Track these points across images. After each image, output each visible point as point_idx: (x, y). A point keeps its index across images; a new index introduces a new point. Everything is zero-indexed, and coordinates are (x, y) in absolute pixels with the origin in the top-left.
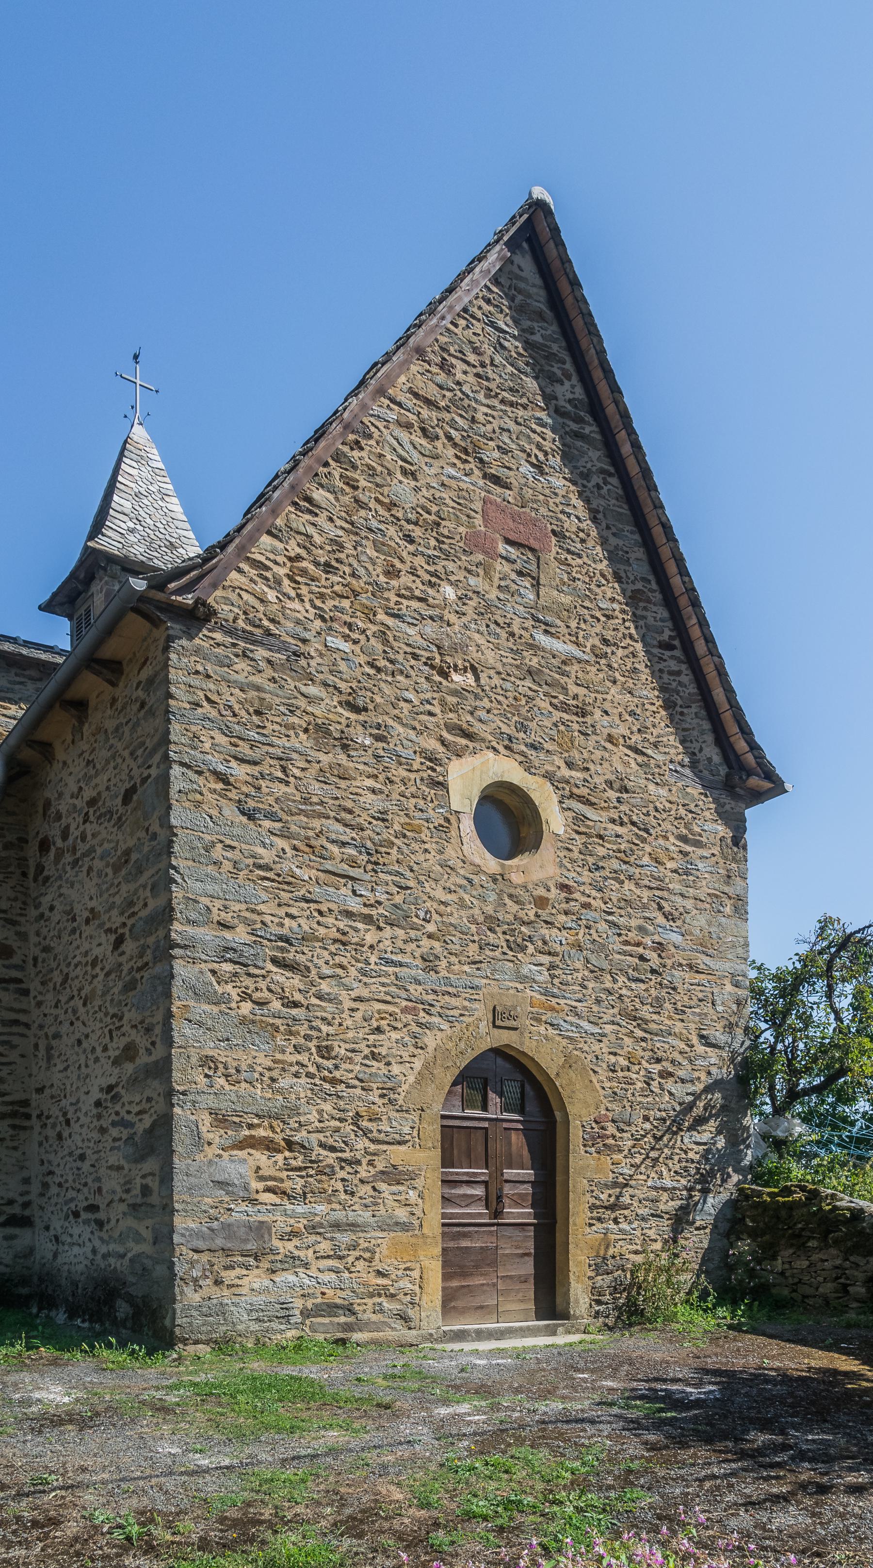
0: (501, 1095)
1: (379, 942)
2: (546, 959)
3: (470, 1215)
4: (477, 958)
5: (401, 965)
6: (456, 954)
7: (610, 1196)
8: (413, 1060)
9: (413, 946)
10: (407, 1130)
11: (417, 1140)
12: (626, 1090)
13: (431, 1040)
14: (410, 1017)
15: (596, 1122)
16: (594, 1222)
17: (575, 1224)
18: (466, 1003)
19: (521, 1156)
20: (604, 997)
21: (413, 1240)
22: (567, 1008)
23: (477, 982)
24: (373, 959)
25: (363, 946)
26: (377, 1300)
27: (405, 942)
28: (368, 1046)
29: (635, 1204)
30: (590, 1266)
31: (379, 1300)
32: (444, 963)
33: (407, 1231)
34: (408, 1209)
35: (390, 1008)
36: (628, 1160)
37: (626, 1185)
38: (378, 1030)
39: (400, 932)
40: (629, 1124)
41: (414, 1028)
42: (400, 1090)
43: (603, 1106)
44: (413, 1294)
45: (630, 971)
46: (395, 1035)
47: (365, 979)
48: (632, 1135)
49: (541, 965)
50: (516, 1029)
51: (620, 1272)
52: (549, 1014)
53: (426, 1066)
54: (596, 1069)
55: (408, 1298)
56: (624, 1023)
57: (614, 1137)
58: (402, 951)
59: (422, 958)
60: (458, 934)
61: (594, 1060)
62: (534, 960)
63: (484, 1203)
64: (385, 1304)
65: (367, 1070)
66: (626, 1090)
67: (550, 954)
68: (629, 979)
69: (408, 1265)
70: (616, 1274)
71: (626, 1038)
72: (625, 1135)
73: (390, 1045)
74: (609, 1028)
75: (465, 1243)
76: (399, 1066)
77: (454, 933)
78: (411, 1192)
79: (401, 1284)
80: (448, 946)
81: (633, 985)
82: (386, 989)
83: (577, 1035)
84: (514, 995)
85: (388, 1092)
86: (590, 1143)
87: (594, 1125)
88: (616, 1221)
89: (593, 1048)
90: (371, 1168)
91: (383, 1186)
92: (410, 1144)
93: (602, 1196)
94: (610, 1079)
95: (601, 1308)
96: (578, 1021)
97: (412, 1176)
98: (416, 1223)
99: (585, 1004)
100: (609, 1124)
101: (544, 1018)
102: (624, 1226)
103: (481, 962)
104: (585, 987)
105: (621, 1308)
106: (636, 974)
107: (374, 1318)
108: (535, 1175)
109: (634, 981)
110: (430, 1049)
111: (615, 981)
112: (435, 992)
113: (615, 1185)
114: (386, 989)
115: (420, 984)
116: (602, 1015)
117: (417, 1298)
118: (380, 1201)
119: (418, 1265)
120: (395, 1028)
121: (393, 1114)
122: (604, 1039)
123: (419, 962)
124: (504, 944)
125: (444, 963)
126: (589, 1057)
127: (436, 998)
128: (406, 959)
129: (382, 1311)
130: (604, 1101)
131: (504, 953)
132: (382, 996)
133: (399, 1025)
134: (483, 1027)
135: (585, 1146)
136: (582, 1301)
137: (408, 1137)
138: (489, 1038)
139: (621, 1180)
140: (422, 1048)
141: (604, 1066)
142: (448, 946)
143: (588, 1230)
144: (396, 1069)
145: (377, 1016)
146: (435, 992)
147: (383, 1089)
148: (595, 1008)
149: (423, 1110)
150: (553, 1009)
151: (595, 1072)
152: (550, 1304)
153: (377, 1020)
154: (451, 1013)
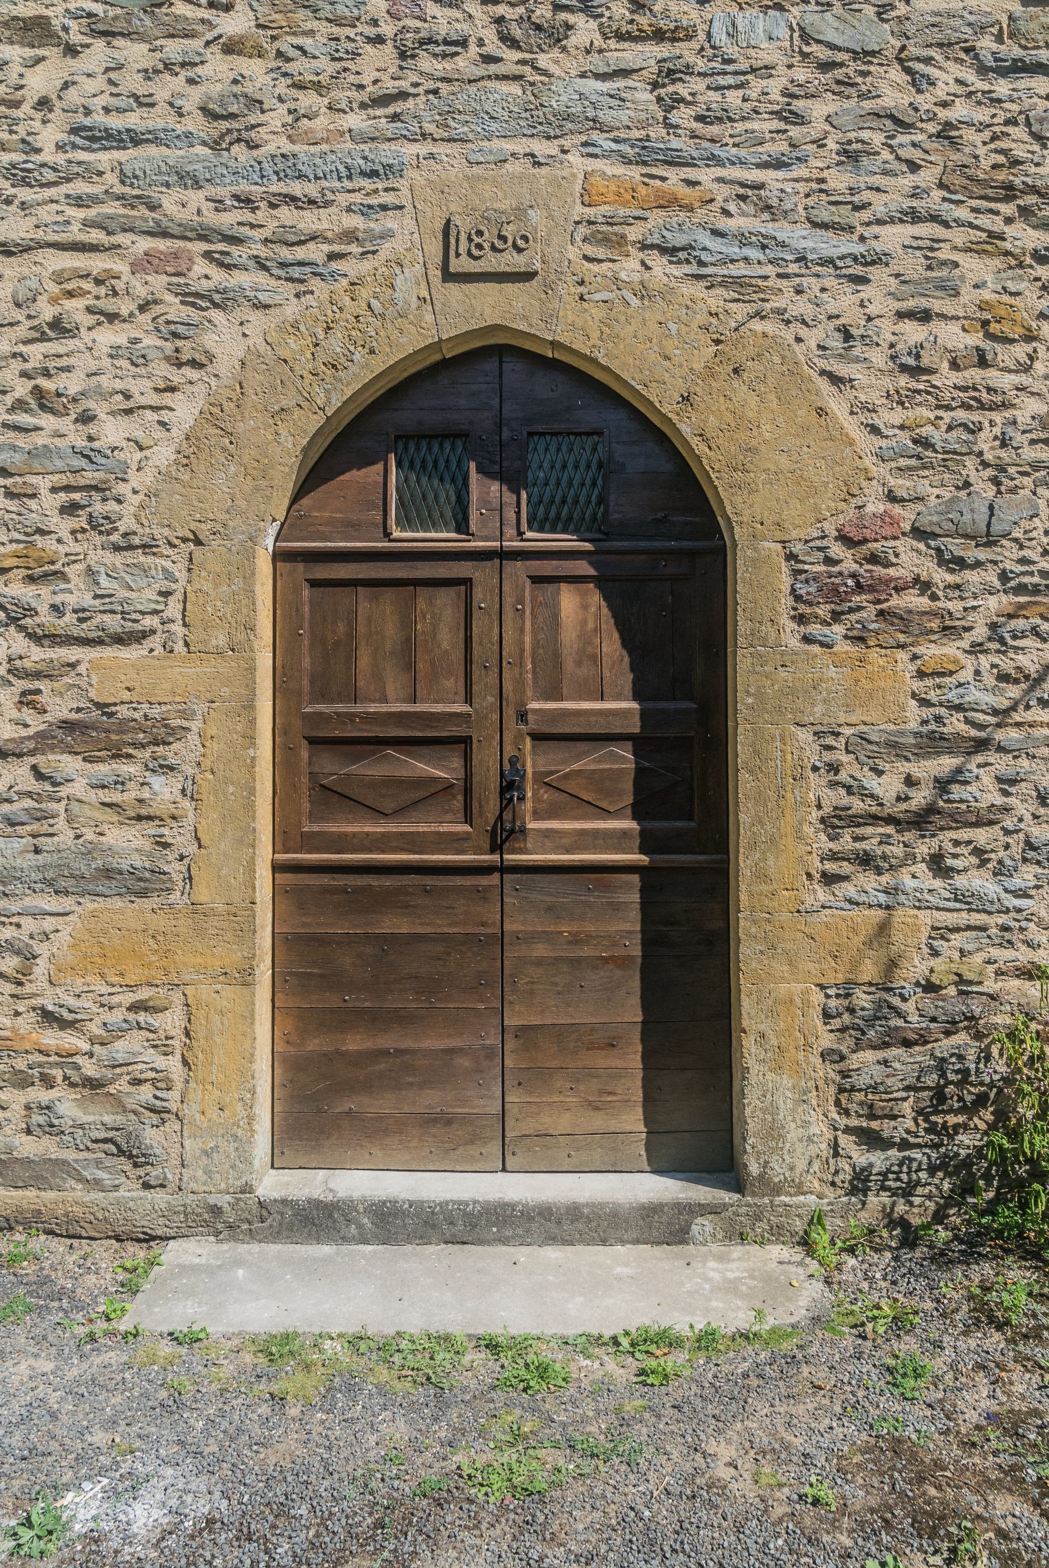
0: (514, 481)
1: (66, 86)
2: (647, 55)
3: (412, 843)
4: (390, 86)
5: (136, 139)
6: (318, 87)
7: (910, 781)
8: (167, 399)
9: (176, 83)
10: (146, 597)
11: (178, 628)
12: (973, 430)
13: (225, 339)
14: (159, 282)
15: (844, 539)
16: (846, 868)
17: (763, 877)
18: (355, 221)
19: (596, 659)
20: (878, 139)
21: (160, 922)
22: (721, 193)
23: (387, 153)
24: (49, 136)
25: (16, 104)
26: (39, 1094)
27: (148, 74)
28: (24, 374)
29: (1022, 809)
30: (827, 1015)
31: (44, 1096)
32: (277, 118)
33: (143, 894)
34: (151, 828)
35: (97, 263)
36: (985, 662)
37: (981, 745)
38: (59, 327)
39: (135, 53)
40: (990, 541)
41: (174, 309)
42: (122, 489)
43: (874, 490)
44: (161, 1081)
45: (986, 44)
46: (108, 337)
47: (25, 194)
48: (1004, 577)
49: (624, 73)
50: (528, 276)
51: (961, 1038)
52: (657, 218)
53: (213, 416)
54: (842, 370)
55: (146, 1093)
56: (963, 213)
57: (924, 586)
58: (144, 102)
59: (203, 109)
60: (325, 29)
61: (836, 343)
62: (595, 62)
63: (458, 802)
64: (62, 1108)
65: (22, 441)
66: (973, 430)
67: (659, 35)
68: (982, 70)
69: (144, 994)
70: (945, 1046)
71: (969, 263)
72: (972, 577)
73: (93, 366)
74: (893, 238)
75: (394, 924)
76: (123, 421)
77: (314, 24)
78: (157, 782)
79: (121, 1048)
80: (289, 67)
81: (1002, 87)
82: (92, 213)
83: (770, 270)
84: (521, 178)
85: (85, 496)
86: (823, 611)
87: (837, 550)
88: (938, 864)
89: (832, 308)
90: (27, 714)
91: (69, 764)
92: (155, 642)
93: (872, 783)
94: (900, 399)
95: (878, 1160)
96: (770, 228)
97: (163, 734)
98: (175, 869)
99: (799, 171)
100: (903, 545)
101: (633, 233)
102: (979, 882)
103: (403, 95)
104: (799, 119)
105: (967, 1164)
106: (1012, 50)
107: (28, 1147)
108: (644, 714)
109: (1003, 72)
110: (225, 366)
111: (918, 82)
112: (245, 201)
113: (933, 743)
114: (92, 213)
115: (197, 185)
116: (867, 196)
117: (174, 1095)
118: (60, 807)
119: (177, 997)
120: (112, 317)
121: (102, 558)
122: (875, 273)
123: (195, 124)
124: (490, 34)
125: (277, 118)
126: (812, 337)
127: (247, 216)
128: (158, 119)
129: (51, 1129)
130: (880, 471)
131: (489, 59)
132: (75, 233)
133: (126, 307)
134: (408, 286)
135: (801, 619)
136: (793, 1133)
137: (149, 622)
138: (424, 316)
139: (956, 724)
140: (194, 364)
141: (878, 358)
142: (289, 67)
143: (822, 895)
144: (112, 431)
145: (53, 288)
146: (245, 201)
147: (68, 488)
148: (839, 180)
149: (198, 542)
150: (668, 203)
151: (835, 380)
152: (700, 1131)
153: (54, 301)
154: (300, 253)
